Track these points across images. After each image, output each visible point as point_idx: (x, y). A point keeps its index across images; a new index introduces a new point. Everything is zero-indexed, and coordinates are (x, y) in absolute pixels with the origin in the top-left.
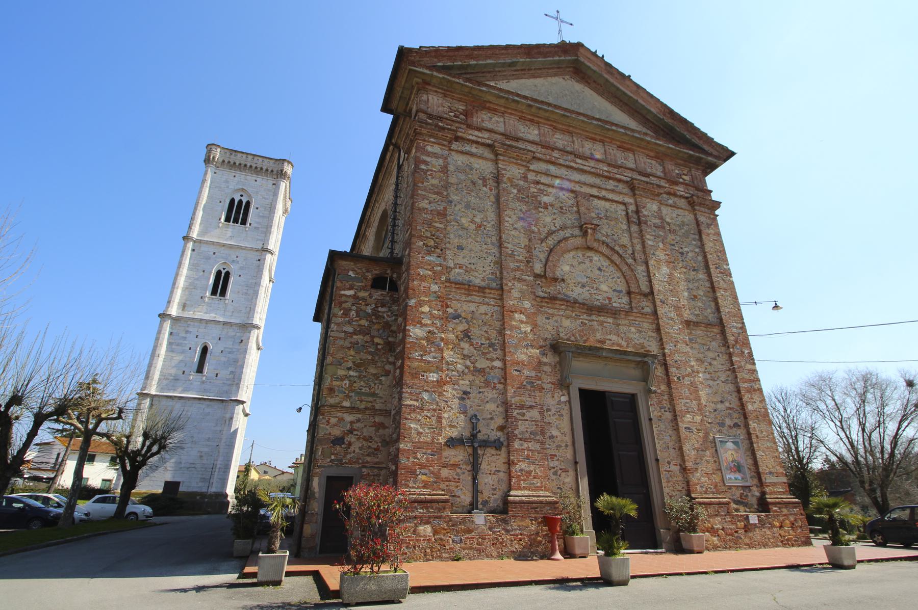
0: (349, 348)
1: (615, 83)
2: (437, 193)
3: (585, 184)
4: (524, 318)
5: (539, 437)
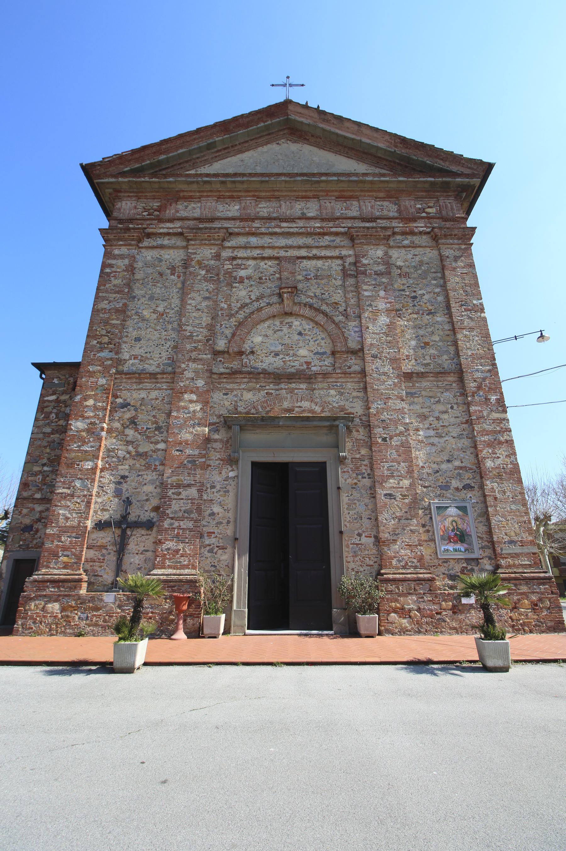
0: (45, 447)
1: (333, 130)
2: (118, 292)
3: (291, 247)
4: (194, 397)
5: (194, 515)
